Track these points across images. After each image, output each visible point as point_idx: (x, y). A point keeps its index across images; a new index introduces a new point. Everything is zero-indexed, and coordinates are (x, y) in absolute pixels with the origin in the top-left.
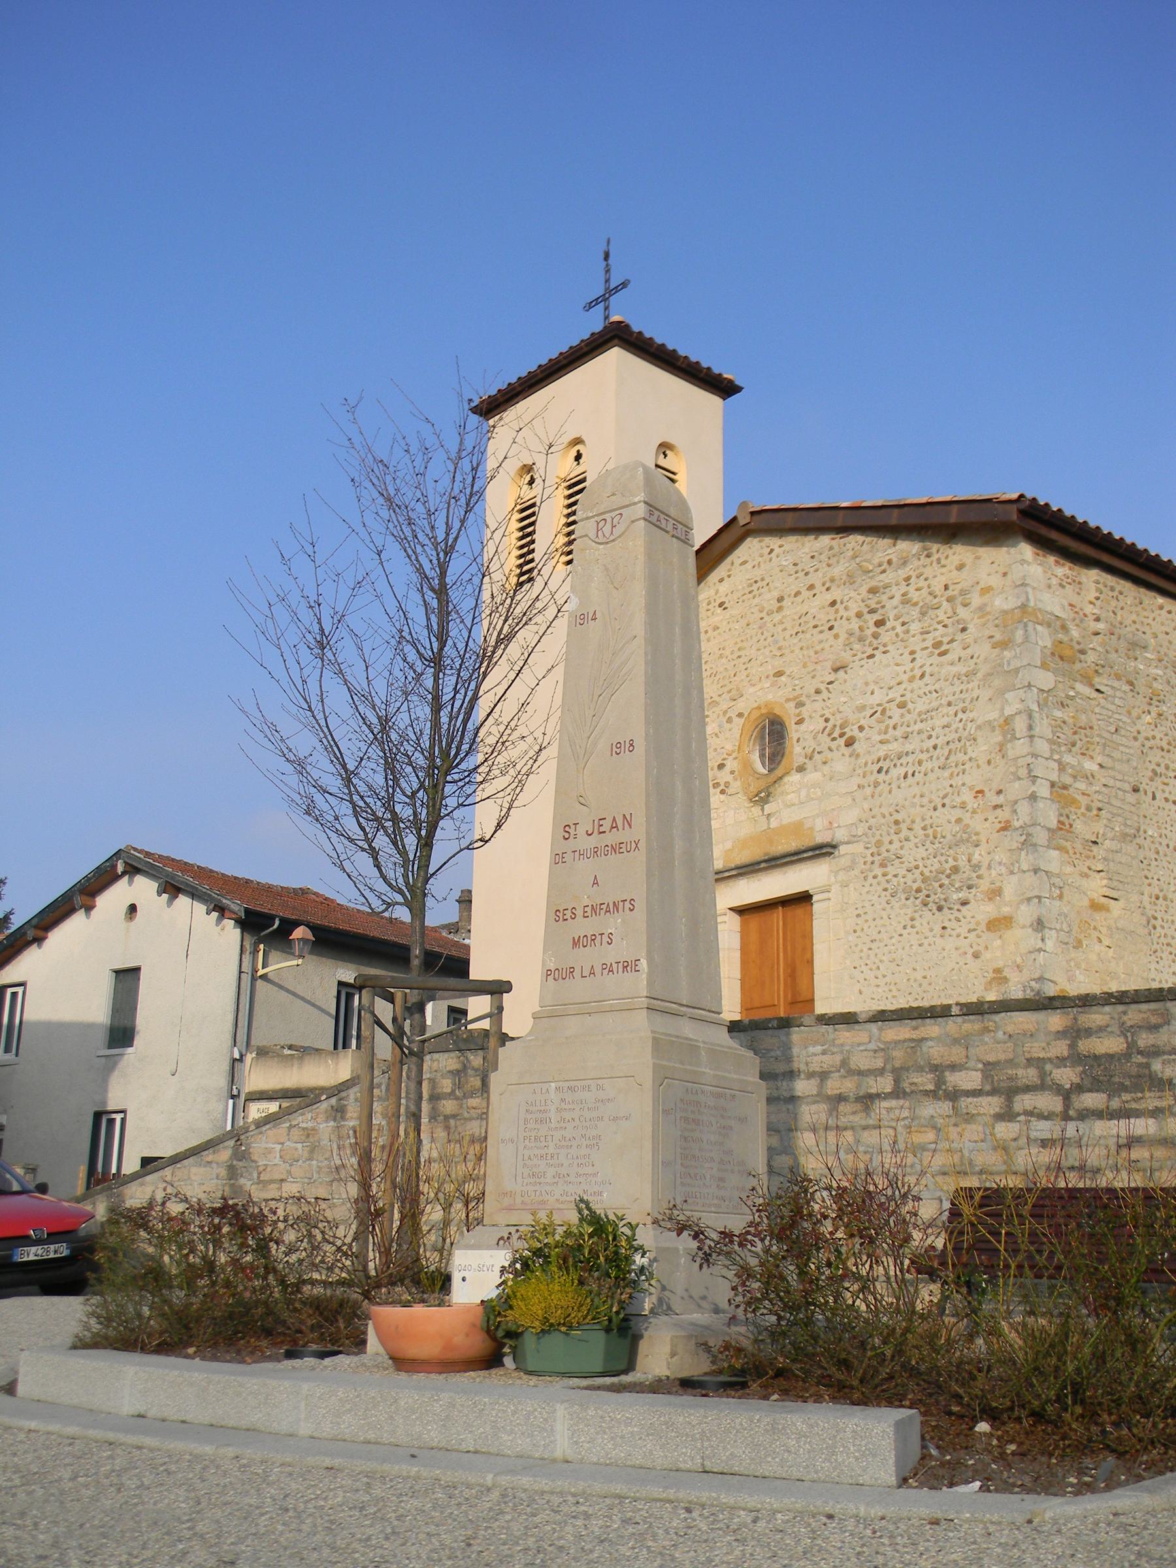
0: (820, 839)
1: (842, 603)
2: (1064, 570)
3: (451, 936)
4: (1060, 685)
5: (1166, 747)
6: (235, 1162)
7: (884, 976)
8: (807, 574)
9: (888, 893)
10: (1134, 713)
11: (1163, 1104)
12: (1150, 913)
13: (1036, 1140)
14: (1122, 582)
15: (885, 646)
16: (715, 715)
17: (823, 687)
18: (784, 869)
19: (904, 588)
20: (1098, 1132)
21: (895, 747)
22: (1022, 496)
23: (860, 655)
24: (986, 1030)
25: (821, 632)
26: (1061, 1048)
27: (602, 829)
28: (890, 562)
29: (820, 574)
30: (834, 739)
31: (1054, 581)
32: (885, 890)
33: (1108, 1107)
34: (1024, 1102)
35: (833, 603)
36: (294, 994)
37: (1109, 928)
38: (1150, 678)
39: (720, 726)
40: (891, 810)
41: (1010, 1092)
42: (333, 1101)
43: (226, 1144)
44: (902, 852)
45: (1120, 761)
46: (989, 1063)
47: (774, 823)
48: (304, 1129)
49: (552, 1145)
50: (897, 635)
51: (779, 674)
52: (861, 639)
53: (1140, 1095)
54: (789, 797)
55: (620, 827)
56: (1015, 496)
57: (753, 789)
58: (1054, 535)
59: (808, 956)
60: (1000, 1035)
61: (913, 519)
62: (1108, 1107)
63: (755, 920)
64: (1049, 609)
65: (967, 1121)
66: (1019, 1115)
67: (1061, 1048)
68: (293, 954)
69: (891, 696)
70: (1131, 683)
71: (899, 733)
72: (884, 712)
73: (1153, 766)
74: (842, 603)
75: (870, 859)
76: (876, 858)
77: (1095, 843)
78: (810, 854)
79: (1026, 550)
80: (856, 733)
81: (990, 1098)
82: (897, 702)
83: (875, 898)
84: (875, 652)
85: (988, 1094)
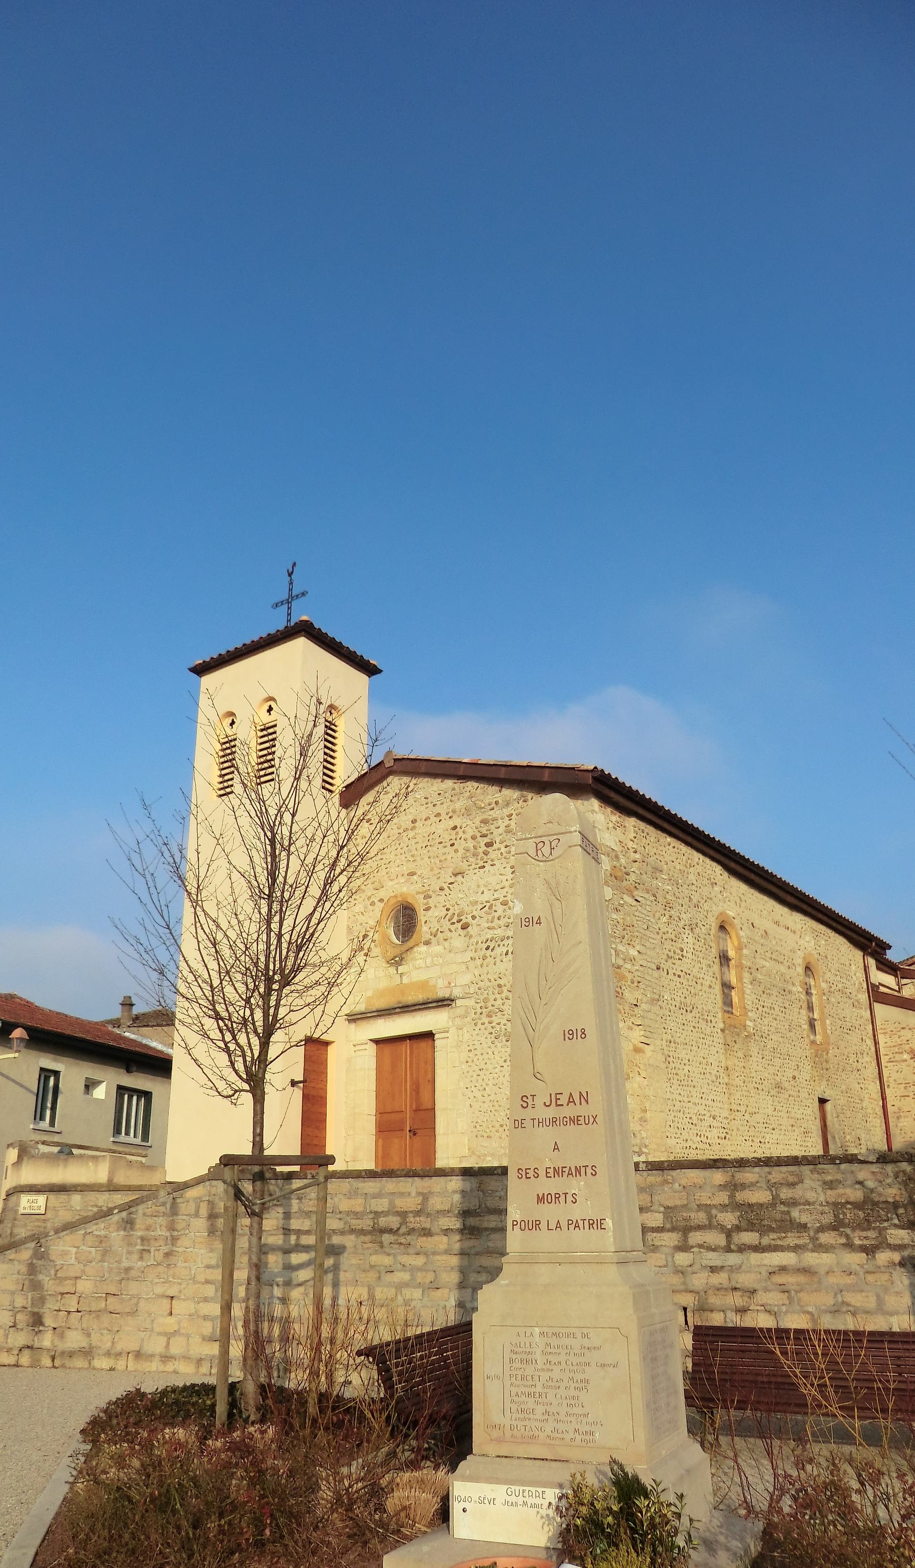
0: (442, 994)
1: (461, 828)
2: (616, 817)
3: (113, 1030)
4: (615, 896)
5: (674, 939)
6: (35, 1261)
7: (489, 1095)
8: (434, 805)
9: (493, 1036)
10: (657, 916)
11: (800, 1242)
12: (666, 1053)
13: (706, 1267)
14: (648, 826)
15: (492, 861)
16: (362, 899)
17: (445, 886)
18: (413, 1013)
19: (507, 822)
20: (753, 1262)
21: (500, 932)
22: (596, 768)
23: (474, 866)
24: (666, 1182)
25: (445, 847)
26: (723, 1198)
27: (559, 1102)
28: (497, 803)
29: (445, 806)
30: (453, 923)
31: (611, 825)
32: (491, 1033)
33: (760, 1243)
34: (696, 1238)
35: (455, 828)
36: (7, 1078)
37: (645, 1065)
38: (665, 892)
39: (365, 907)
40: (496, 976)
41: (686, 1230)
42: (124, 1214)
43: (27, 1245)
44: (504, 1007)
45: (651, 949)
46: (669, 1207)
47: (405, 980)
48: (97, 1236)
49: (539, 1385)
50: (502, 854)
51: (412, 874)
52: (475, 855)
53: (783, 1235)
54: (418, 962)
55: (577, 1101)
56: (591, 767)
57: (390, 955)
58: (612, 795)
59: (430, 1076)
60: (676, 1185)
61: (518, 776)
62: (760, 1243)
63: (388, 1049)
64: (608, 844)
65: (653, 1251)
66: (692, 1247)
67: (723, 1198)
68: (11, 1048)
69: (496, 896)
70: (654, 896)
71: (502, 922)
72: (491, 907)
73: (666, 952)
74: (461, 828)
75: (479, 1011)
76: (484, 1010)
77: (636, 1005)
78: (434, 1004)
79: (595, 803)
80: (470, 920)
81: (670, 1234)
82: (501, 900)
83: (483, 1039)
84: (485, 864)
85: (669, 1231)
